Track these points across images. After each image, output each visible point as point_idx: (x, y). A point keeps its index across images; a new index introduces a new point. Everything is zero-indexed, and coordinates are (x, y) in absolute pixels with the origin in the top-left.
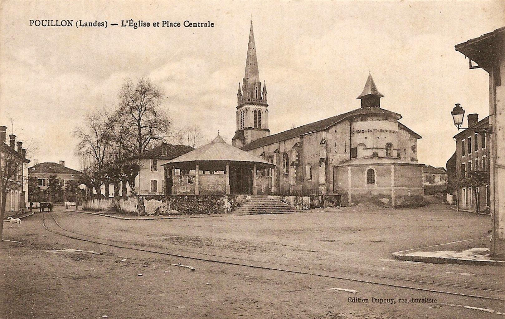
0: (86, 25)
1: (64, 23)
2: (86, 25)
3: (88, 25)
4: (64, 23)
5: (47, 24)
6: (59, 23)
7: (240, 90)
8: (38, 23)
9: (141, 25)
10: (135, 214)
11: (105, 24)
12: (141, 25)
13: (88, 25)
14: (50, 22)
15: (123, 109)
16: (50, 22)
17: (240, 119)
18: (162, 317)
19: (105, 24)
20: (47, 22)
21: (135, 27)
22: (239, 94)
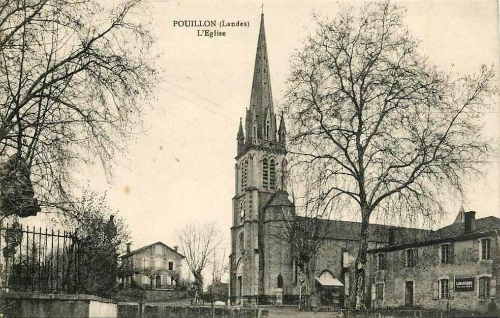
0: (229, 24)
1: (207, 24)
2: (229, 24)
3: (231, 25)
4: (207, 24)
5: (191, 25)
6: (203, 24)
7: (241, 128)
8: (181, 24)
9: (216, 34)
10: (263, 271)
11: (247, 24)
12: (216, 34)
13: (231, 25)
14: (194, 22)
15: (439, 135)
16: (194, 22)
17: (240, 178)
18: (62, 2)
19: (247, 24)
20: (191, 22)
21: (211, 36)
22: (240, 134)
